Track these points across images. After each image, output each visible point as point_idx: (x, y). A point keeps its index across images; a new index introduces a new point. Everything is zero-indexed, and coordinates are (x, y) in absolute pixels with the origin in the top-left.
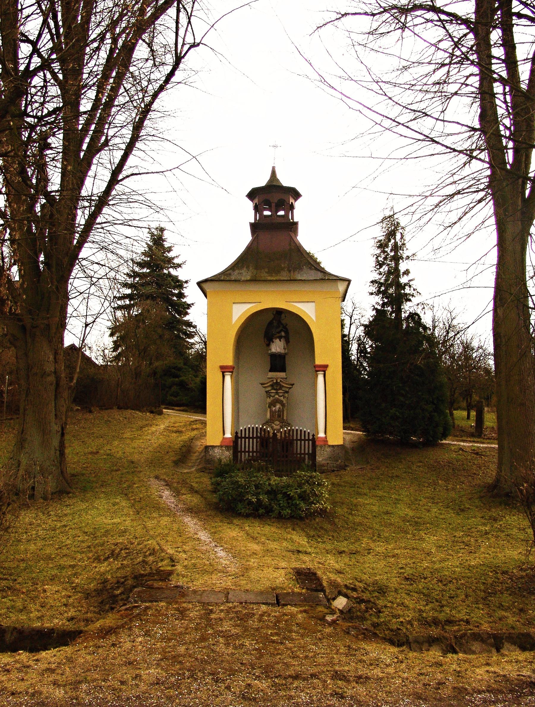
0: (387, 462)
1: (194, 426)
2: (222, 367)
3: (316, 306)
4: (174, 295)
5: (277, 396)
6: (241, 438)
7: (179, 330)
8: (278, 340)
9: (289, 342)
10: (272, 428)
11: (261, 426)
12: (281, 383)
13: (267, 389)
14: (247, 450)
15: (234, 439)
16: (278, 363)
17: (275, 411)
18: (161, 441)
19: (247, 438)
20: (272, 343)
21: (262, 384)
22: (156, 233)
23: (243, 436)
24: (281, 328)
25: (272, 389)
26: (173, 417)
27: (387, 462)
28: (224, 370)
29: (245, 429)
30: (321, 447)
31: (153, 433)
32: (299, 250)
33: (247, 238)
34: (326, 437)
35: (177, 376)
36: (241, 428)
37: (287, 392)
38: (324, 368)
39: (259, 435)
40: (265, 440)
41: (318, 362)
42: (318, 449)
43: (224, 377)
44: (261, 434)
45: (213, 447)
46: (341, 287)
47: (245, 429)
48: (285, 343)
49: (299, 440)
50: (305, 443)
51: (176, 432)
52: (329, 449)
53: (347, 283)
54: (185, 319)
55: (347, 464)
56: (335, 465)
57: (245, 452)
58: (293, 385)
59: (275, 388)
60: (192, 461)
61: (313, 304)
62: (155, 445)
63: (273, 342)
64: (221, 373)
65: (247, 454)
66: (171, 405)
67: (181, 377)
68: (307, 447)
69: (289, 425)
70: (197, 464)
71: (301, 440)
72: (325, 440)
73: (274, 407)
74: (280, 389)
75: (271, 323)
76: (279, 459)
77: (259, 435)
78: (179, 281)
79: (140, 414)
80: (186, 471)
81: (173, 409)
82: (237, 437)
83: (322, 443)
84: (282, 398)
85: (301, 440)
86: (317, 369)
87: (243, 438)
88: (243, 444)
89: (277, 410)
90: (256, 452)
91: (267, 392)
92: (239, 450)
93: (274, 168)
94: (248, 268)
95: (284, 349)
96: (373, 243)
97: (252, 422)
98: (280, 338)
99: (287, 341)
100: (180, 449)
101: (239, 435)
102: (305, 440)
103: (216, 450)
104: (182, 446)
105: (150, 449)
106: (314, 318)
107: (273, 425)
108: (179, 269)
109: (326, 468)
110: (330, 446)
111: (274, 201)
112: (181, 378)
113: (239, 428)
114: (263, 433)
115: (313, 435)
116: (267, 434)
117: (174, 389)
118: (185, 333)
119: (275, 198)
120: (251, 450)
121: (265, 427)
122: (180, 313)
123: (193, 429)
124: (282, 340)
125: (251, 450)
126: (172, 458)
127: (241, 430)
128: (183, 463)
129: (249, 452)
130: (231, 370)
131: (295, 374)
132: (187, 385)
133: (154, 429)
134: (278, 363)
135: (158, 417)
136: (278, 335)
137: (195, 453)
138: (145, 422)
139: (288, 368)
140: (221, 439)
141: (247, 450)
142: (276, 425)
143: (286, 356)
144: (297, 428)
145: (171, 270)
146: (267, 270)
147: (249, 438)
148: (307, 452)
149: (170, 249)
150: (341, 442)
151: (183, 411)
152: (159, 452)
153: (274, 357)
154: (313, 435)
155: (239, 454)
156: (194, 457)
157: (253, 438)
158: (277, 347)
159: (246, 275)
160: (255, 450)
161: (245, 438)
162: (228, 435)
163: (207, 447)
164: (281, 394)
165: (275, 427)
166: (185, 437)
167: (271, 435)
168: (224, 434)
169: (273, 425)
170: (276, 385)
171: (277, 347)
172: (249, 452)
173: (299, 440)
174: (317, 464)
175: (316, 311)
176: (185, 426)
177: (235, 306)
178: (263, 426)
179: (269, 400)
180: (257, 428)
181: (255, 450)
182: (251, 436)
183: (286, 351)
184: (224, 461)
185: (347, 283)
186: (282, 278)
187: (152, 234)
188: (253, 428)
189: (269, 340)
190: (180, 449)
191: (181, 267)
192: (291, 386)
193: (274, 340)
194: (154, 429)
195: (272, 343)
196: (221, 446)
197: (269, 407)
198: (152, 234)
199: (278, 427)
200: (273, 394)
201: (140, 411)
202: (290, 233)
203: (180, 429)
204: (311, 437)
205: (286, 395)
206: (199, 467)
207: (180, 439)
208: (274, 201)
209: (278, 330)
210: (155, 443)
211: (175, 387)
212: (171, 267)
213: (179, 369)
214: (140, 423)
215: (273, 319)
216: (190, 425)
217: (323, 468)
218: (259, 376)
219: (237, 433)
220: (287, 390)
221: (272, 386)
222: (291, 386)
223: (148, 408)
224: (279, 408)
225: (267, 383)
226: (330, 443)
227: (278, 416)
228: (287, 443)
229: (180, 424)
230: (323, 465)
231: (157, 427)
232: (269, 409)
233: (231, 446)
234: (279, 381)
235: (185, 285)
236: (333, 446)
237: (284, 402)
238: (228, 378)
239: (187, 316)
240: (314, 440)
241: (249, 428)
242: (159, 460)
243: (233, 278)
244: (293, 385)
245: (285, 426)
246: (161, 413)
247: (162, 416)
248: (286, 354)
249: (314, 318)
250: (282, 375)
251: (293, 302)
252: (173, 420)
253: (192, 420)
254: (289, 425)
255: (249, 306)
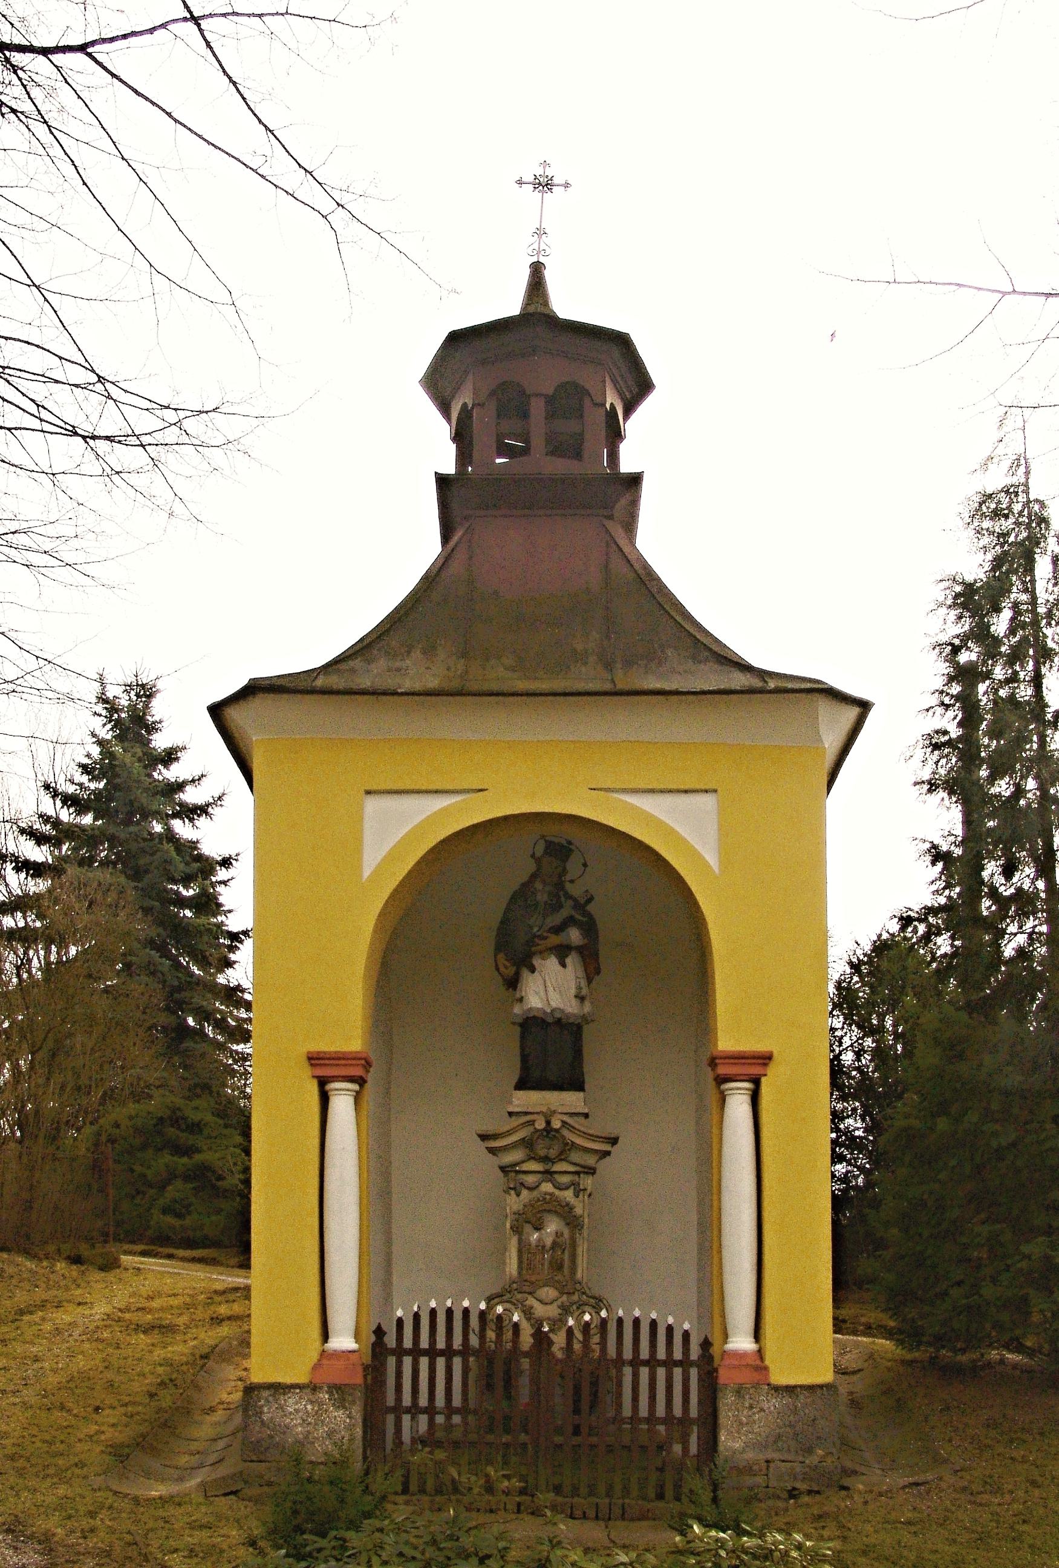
0: (1024, 1460)
1: (223, 1310)
2: (314, 1059)
3: (721, 810)
4: (182, 903)
5: (547, 1187)
6: (400, 1352)
7: (205, 1015)
8: (552, 962)
9: (598, 971)
10: (528, 1313)
11: (483, 1306)
12: (565, 1132)
13: (509, 1158)
14: (423, 1402)
15: (367, 1359)
16: (551, 1054)
17: (541, 1247)
18: (81, 1362)
19: (425, 1352)
20: (525, 973)
21: (484, 1137)
22: (124, 702)
23: (408, 1343)
24: (566, 911)
25: (530, 1158)
26: (159, 1279)
27: (1024, 1460)
28: (325, 1070)
29: (417, 1317)
30: (739, 1392)
31: (58, 1331)
32: (647, 585)
33: (424, 546)
34: (760, 1352)
35: (187, 1151)
36: (399, 1313)
37: (591, 1171)
38: (753, 1068)
39: (474, 1341)
40: (495, 1361)
41: (726, 1043)
42: (727, 1402)
43: (325, 1099)
44: (482, 1336)
45: (278, 1389)
46: (832, 725)
47: (417, 1317)
48: (581, 973)
49: (646, 1363)
50: (636, 1375)
51: (148, 1329)
52: (773, 1404)
53: (854, 712)
54: (221, 979)
55: (849, 1464)
56: (798, 1468)
57: (414, 1410)
58: (614, 1141)
59: (542, 1153)
60: (194, 1446)
61: (707, 802)
62: (53, 1380)
63: (533, 970)
64: (313, 1088)
65: (423, 1419)
66: (161, 1243)
67: (199, 1151)
68: (681, 1395)
69: (598, 1303)
70: (213, 1458)
71: (636, 1363)
72: (758, 1362)
73: (538, 1229)
74: (562, 1157)
75: (522, 895)
76: (558, 1439)
77: (474, 1341)
78: (200, 858)
79: (30, 1264)
80: (158, 1490)
81: (170, 1256)
82: (380, 1347)
83: (745, 1377)
84: (568, 1195)
85: (636, 1363)
86: (722, 1070)
87: (408, 1352)
88: (409, 1379)
89: (549, 1242)
90: (463, 1411)
91: (503, 1169)
92: (391, 1401)
93: (537, 270)
94: (430, 651)
95: (581, 998)
96: (941, 593)
97: (445, 1288)
98: (562, 952)
99: (591, 960)
100: (152, 1395)
101: (391, 1341)
102: (652, 1362)
103: (291, 1403)
104: (162, 1384)
105: (29, 1395)
106: (712, 859)
107: (531, 1301)
108: (202, 821)
109: (760, 1480)
110: (777, 1389)
111: (536, 403)
112: (198, 1157)
113: (393, 1311)
114: (491, 1335)
115: (706, 1344)
116: (508, 1335)
117: (176, 1190)
118: (220, 1025)
119: (544, 376)
120: (440, 1401)
121: (500, 1309)
122: (203, 961)
123: (217, 1320)
124: (569, 961)
125: (440, 1401)
126: (109, 1434)
127: (400, 1321)
128: (154, 1451)
129: (431, 1410)
130: (358, 1072)
131: (626, 1094)
132: (220, 1178)
133: (63, 1317)
134: (551, 1054)
135: (96, 1275)
136: (554, 940)
137: (212, 1410)
138: (40, 1294)
139: (586, 1087)
140: (313, 1355)
141: (423, 1402)
142: (545, 1304)
143: (586, 1029)
144: (637, 1313)
145: (177, 825)
146: (509, 661)
147: (432, 1353)
148: (661, 1411)
149: (170, 757)
150: (825, 1375)
151: (193, 1260)
152: (62, 1407)
153: (533, 1026)
154: (706, 1344)
155: (390, 1419)
156: (205, 1428)
157: (449, 1353)
158: (550, 988)
159: (419, 673)
160: (457, 1402)
161: (416, 1352)
162: (343, 1341)
163: (250, 1390)
164: (565, 1179)
165: (540, 1310)
166: (178, 1349)
167: (527, 1340)
168: (325, 1336)
169: (531, 1301)
170: (547, 1142)
171: (550, 988)
172: (431, 1410)
173: (646, 1363)
174: (719, 1461)
175: (724, 832)
176: (187, 1306)
177: (372, 805)
178: (490, 1308)
179: (514, 1203)
180: (466, 1311)
181: (457, 1402)
182: (441, 1344)
183: (587, 1008)
184: (320, 1449)
185: (854, 712)
186: (581, 686)
187: (111, 706)
188: (449, 1312)
189: (516, 958)
190: (152, 1395)
191: (207, 813)
192: (606, 1147)
193: (536, 962)
194: (68, 1318)
195: (525, 973)
196: (313, 1387)
197: (517, 1229)
198: (111, 706)
199: (553, 1311)
200: (530, 1179)
201: (27, 1253)
202: (609, 524)
203: (168, 1318)
204: (695, 1353)
205: (588, 1182)
206: (223, 1471)
207: (159, 1354)
208: (536, 403)
209: (556, 919)
210: (55, 1371)
211: (179, 1183)
212: (175, 815)
213: (195, 1128)
214: (21, 1298)
215: (534, 876)
216: (210, 1301)
217: (749, 1481)
218: (474, 1100)
219: (379, 1332)
220: (591, 1160)
221: (527, 1144)
222: (606, 1147)
223: (63, 1247)
224: (558, 1234)
225: (508, 1133)
226: (780, 1377)
227: (556, 1266)
228: (587, 1378)
229: (174, 1302)
230: (748, 1470)
231: (80, 1309)
232: (514, 1241)
233: (353, 1387)
234: (556, 1124)
235: (222, 874)
236: (790, 1389)
237: (578, 1211)
238: (342, 1104)
239: (229, 972)
240: (707, 1363)
241: (433, 1312)
242: (50, 1443)
243: (365, 682)
244: (614, 1141)
245: (581, 1306)
246: (109, 1265)
247: (111, 1276)
248: (586, 1019)
249: (712, 859)
250: (571, 1100)
251: (624, 791)
252: (147, 1286)
253: (219, 1286)
254: (598, 1303)
255: (439, 803)
